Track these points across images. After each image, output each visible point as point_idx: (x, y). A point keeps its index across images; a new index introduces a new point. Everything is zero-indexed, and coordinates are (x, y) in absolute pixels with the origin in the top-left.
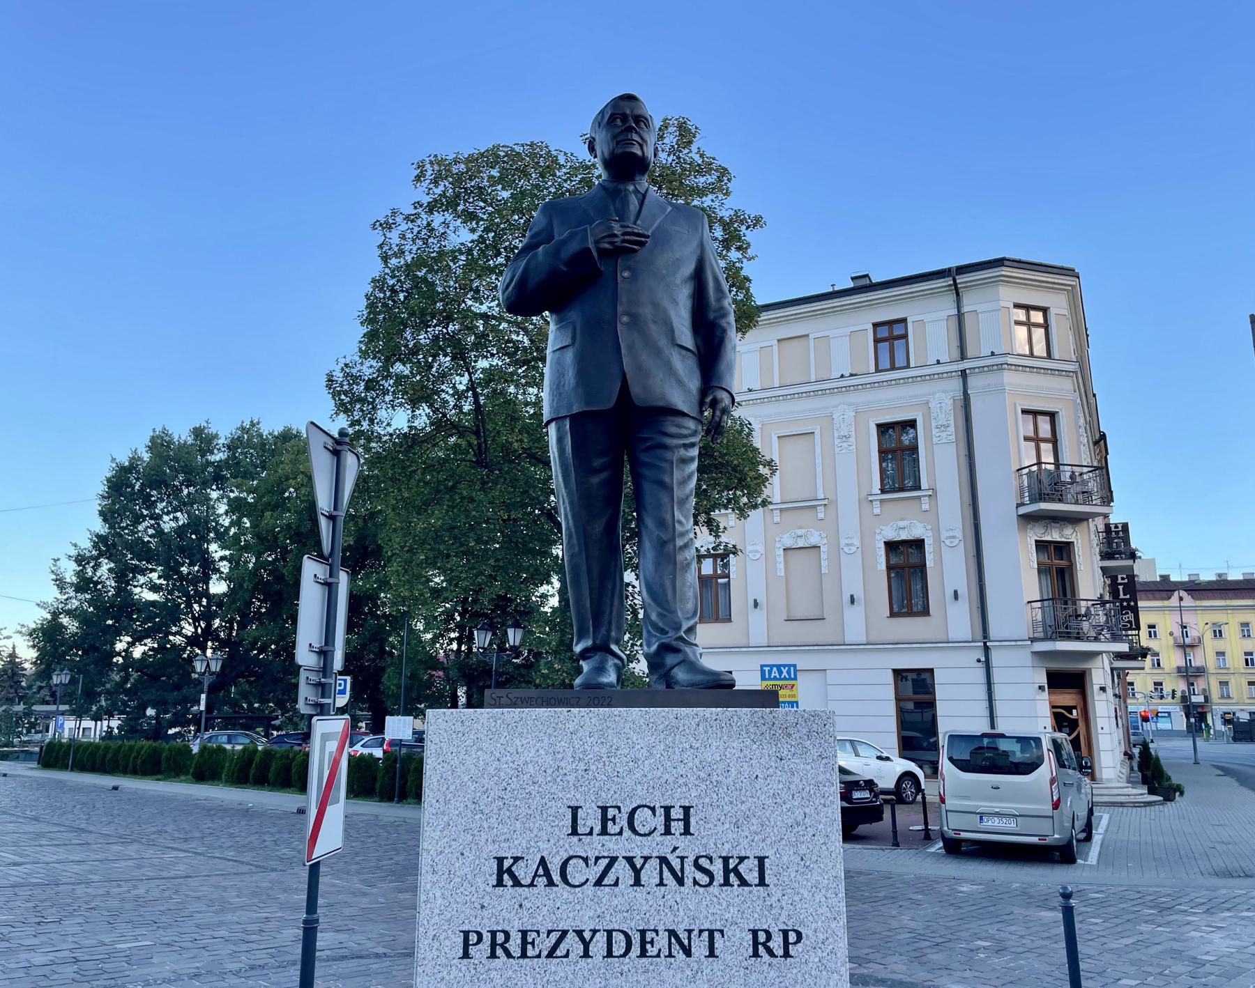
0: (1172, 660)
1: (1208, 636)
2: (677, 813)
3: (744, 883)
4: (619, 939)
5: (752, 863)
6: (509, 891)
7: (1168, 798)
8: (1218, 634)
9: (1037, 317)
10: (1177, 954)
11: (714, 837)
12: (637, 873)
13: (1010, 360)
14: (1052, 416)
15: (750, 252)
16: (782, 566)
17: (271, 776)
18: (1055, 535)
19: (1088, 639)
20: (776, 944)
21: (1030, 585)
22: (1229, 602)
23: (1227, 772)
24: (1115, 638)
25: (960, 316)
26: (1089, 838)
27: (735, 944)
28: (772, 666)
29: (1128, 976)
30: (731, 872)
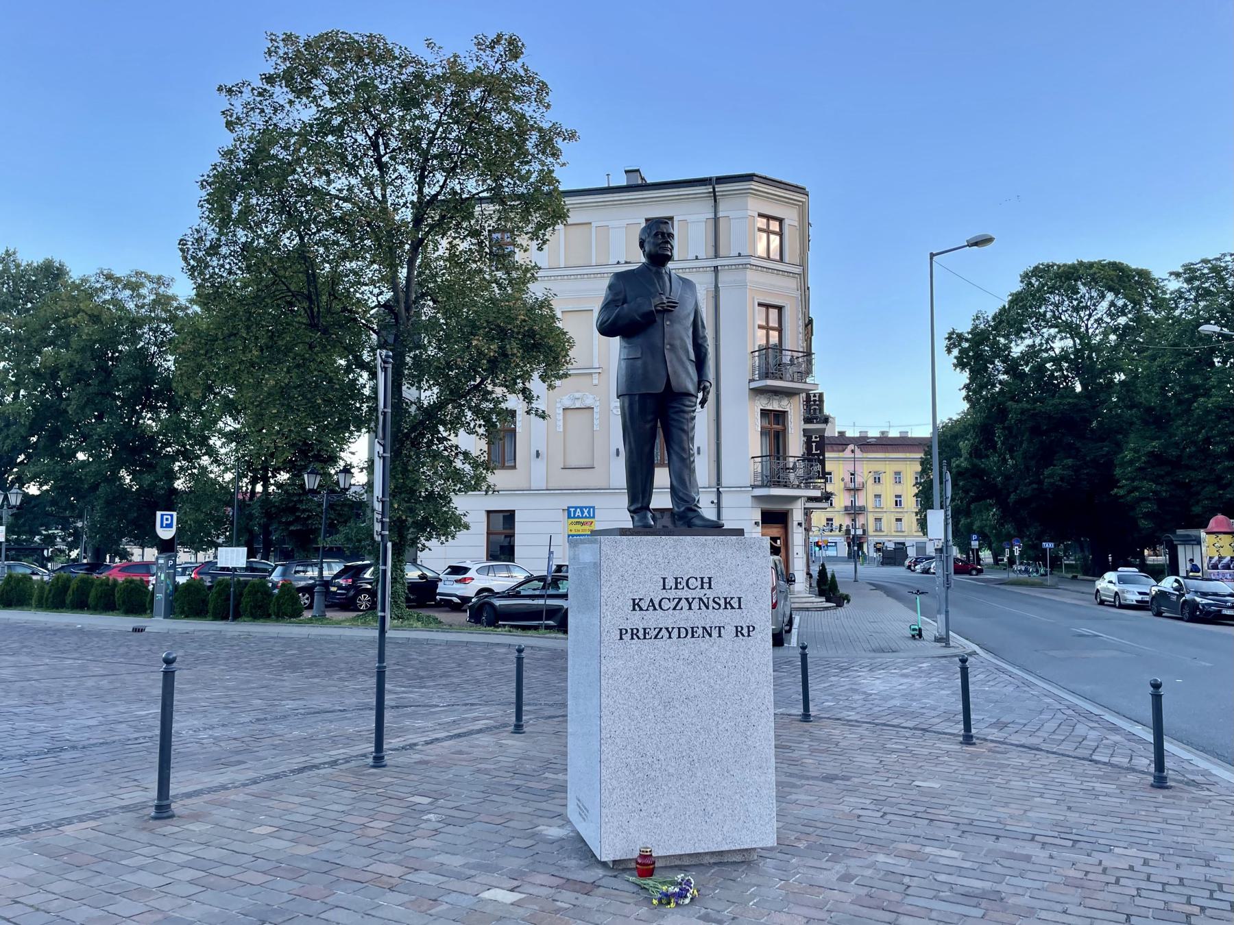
0: (841, 500)
1: (871, 481)
2: (706, 580)
3: (732, 608)
4: (683, 630)
5: (736, 600)
6: (638, 612)
7: (839, 605)
8: (877, 480)
9: (775, 226)
10: (855, 691)
11: (721, 589)
12: (690, 604)
13: (753, 261)
14: (780, 309)
15: (562, 159)
16: (561, 423)
17: (91, 600)
18: (775, 406)
19: (793, 487)
20: (745, 631)
21: (755, 444)
22: (888, 455)
23: (877, 587)
24: (807, 487)
25: (716, 220)
26: (789, 631)
27: (729, 632)
28: (576, 508)
29: (827, 701)
30: (634, 634)
